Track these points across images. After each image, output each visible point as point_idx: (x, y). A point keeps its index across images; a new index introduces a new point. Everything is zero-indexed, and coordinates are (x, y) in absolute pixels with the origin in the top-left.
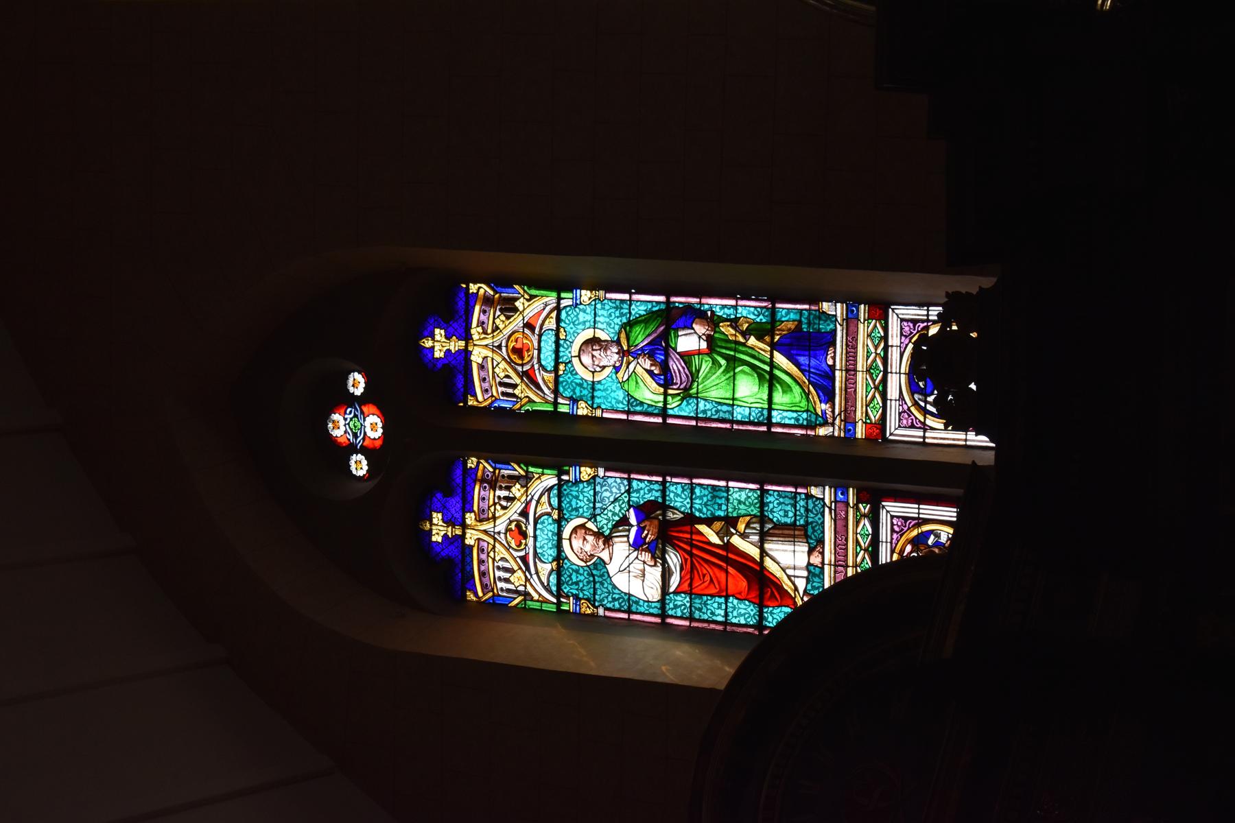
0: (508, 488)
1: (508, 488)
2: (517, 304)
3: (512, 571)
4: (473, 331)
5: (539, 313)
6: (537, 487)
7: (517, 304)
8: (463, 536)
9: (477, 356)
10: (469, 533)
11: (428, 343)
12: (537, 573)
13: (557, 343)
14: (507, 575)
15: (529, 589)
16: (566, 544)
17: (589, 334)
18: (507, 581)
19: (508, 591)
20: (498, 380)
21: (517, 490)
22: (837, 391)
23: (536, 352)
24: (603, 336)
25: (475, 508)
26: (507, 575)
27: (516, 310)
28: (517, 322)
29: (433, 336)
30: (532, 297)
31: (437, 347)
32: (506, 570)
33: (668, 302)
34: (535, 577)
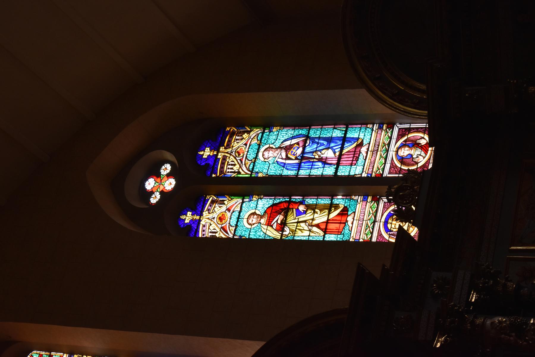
0: (241, 136)
1: (241, 136)
2: (225, 202)
3: (235, 165)
4: (204, 213)
5: (234, 205)
6: (253, 134)
7: (225, 202)
8: (217, 155)
9: (203, 223)
10: (220, 154)
11: (183, 217)
12: (245, 164)
13: (238, 218)
14: (232, 167)
15: (240, 170)
16: (260, 154)
17: (253, 211)
18: (232, 169)
19: (231, 172)
20: (210, 231)
21: (245, 136)
22: (375, 88)
23: (229, 219)
24: (258, 212)
25: (225, 144)
26: (232, 167)
27: (224, 204)
28: (224, 208)
29: (186, 215)
30: (232, 199)
31: (187, 218)
32: (232, 165)
33: (290, 199)
34: (244, 166)
